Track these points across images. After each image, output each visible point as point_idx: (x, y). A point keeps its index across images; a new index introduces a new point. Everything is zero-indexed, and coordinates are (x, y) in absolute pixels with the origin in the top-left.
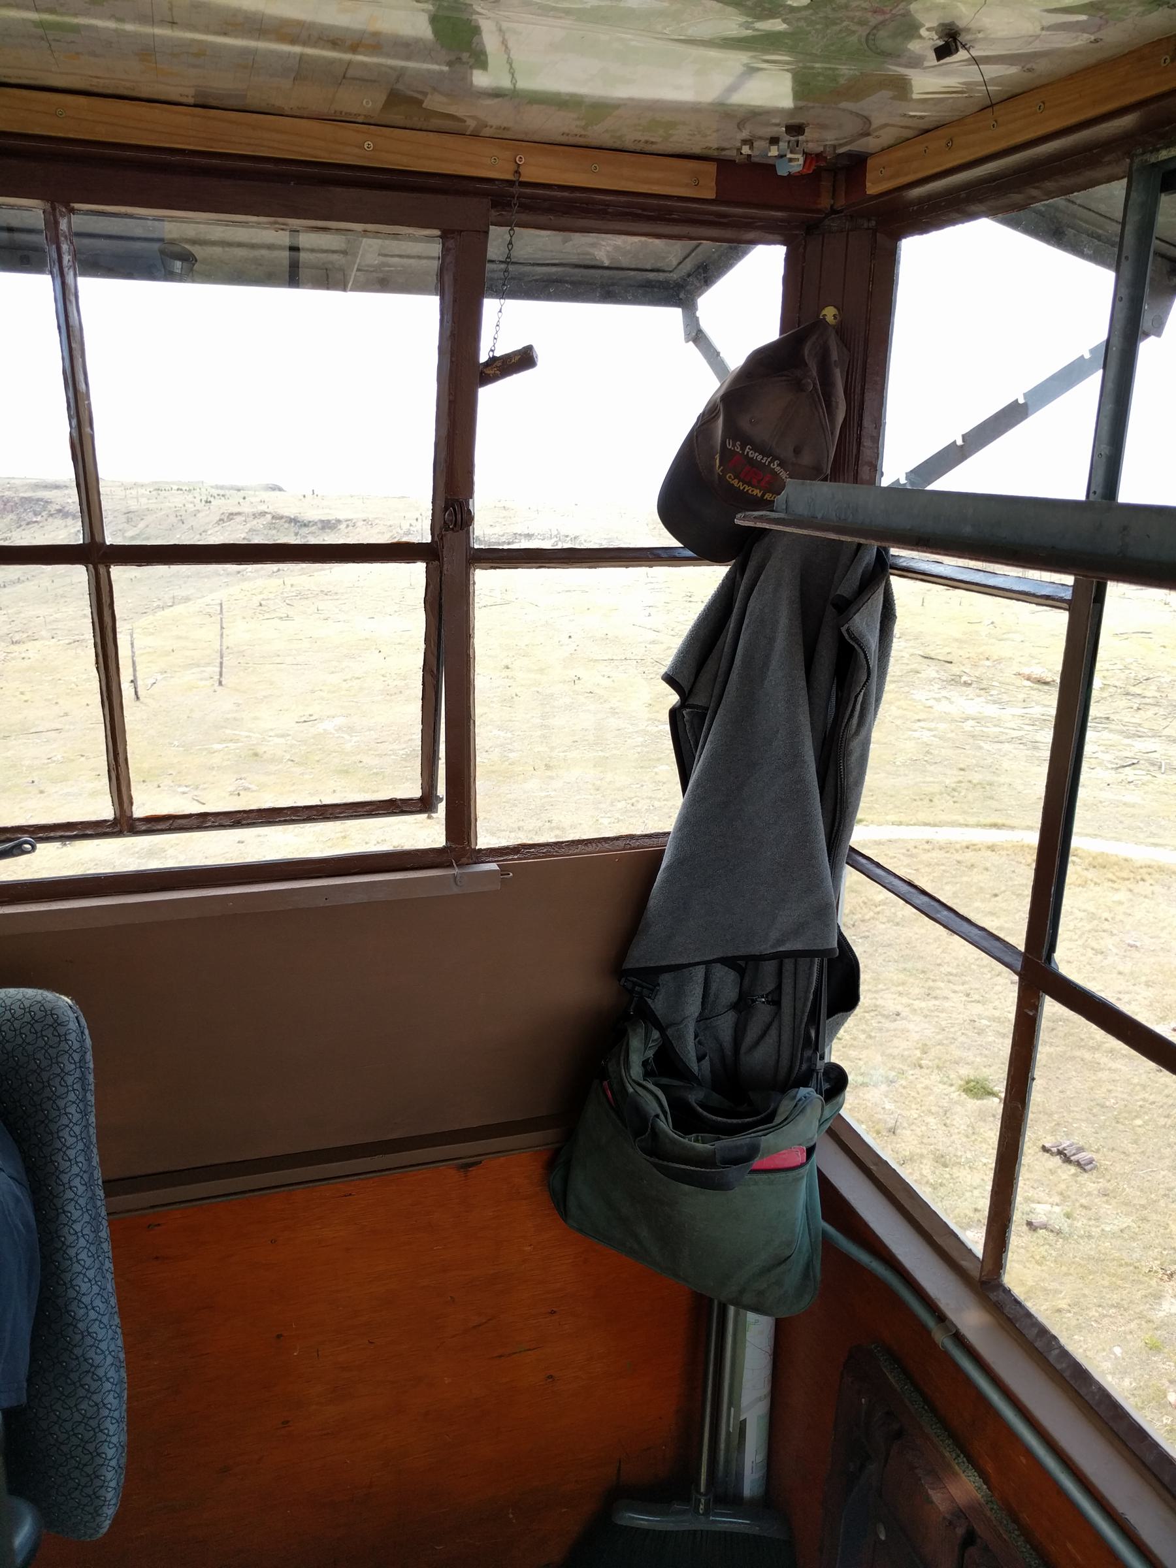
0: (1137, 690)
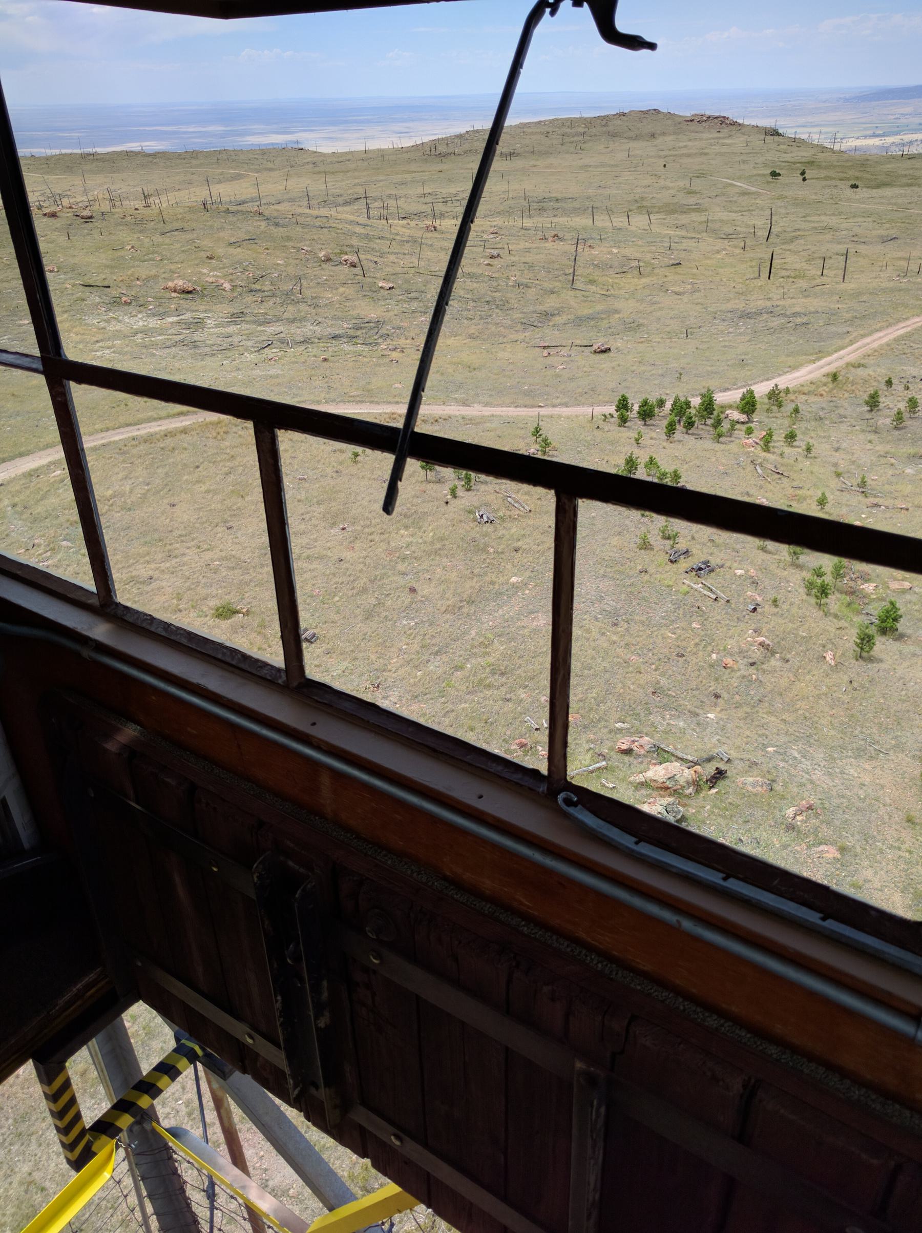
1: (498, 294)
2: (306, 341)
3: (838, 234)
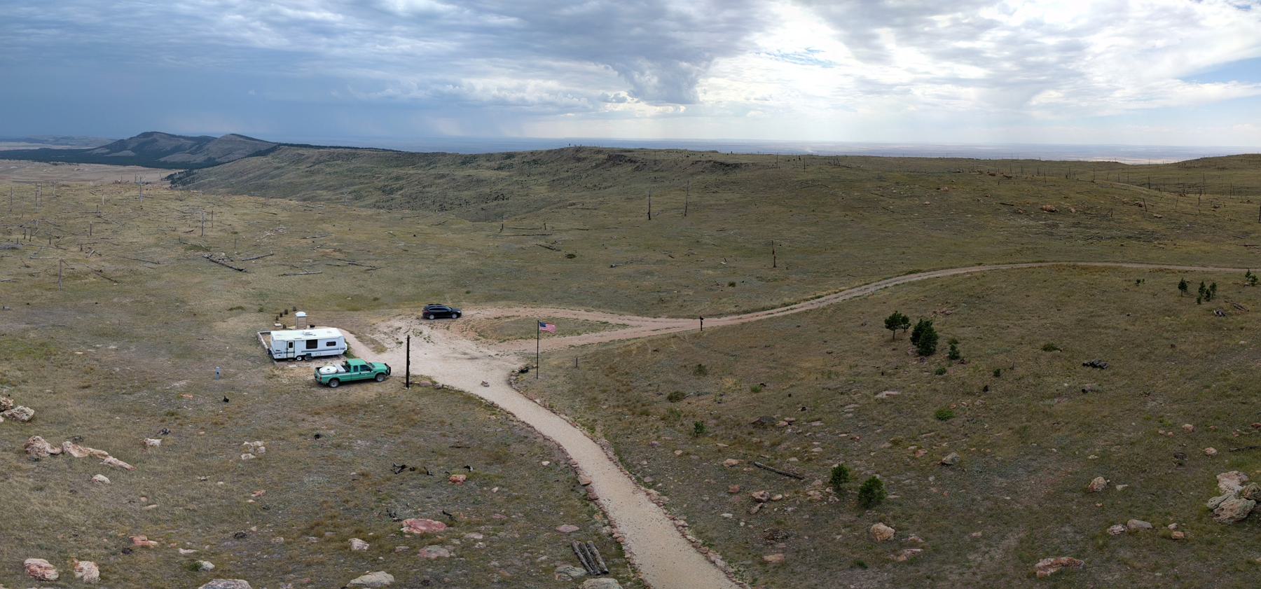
0: (1089, 212)
2: (1112, 238)
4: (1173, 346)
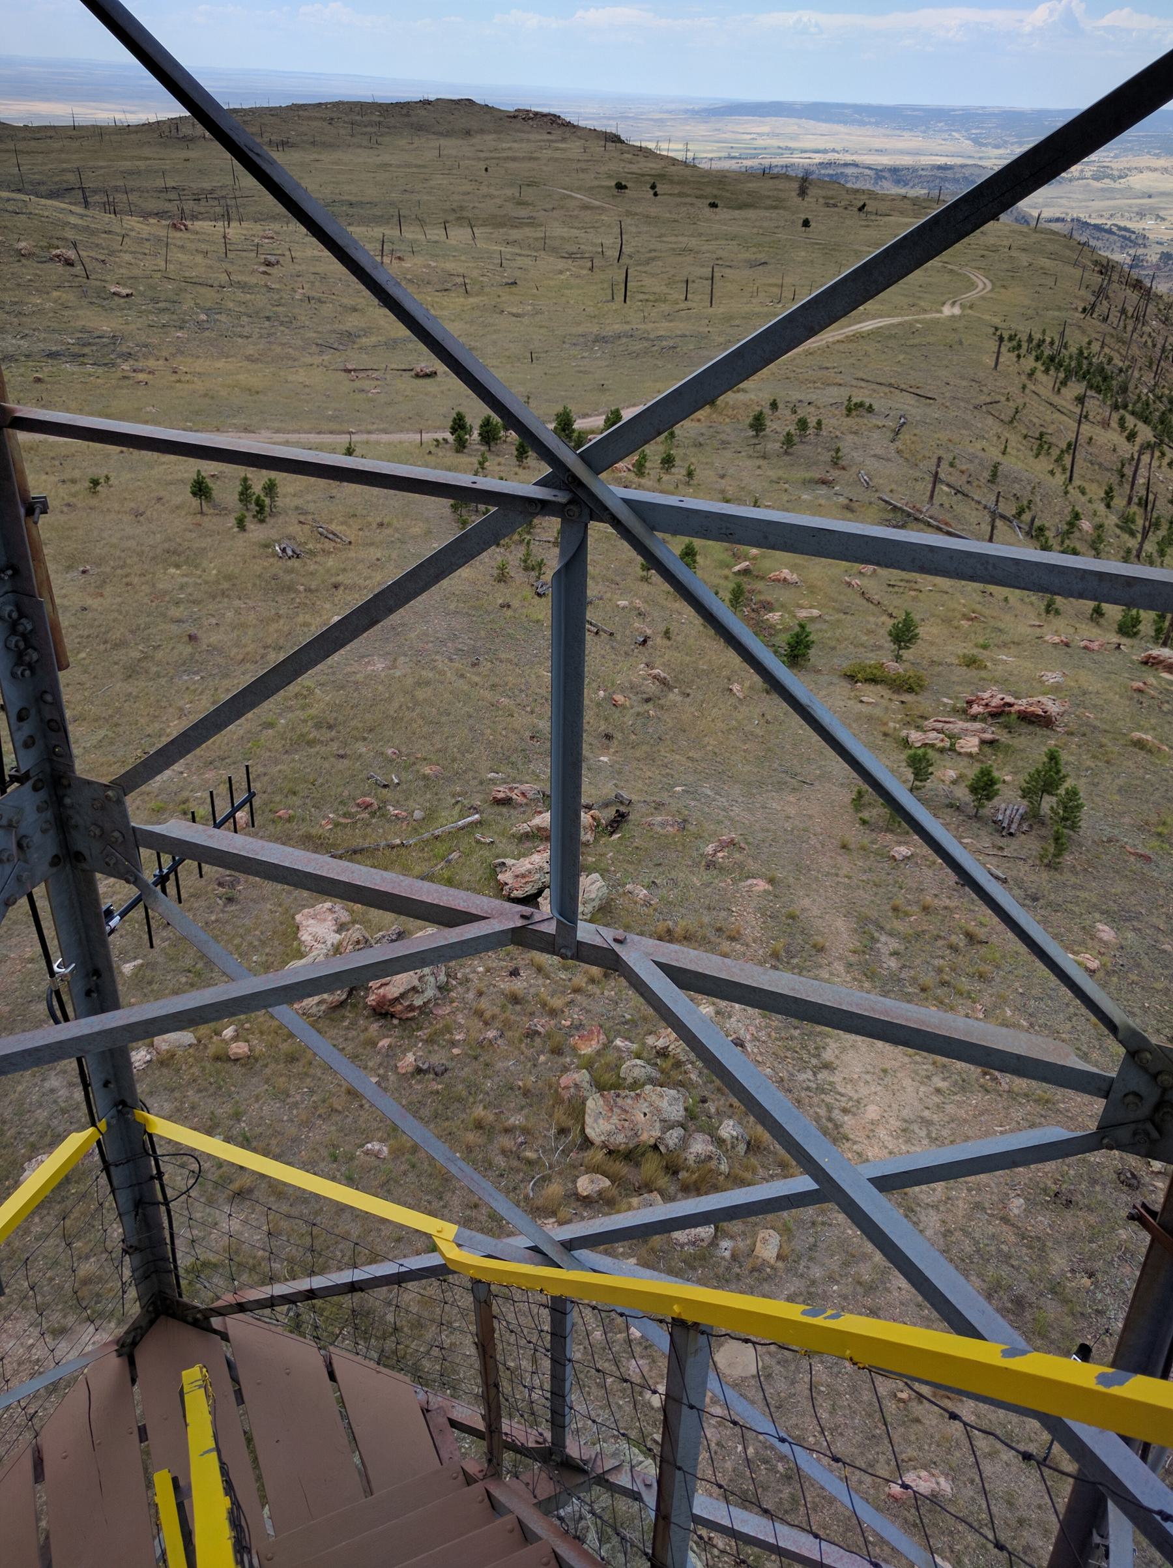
1: (280, 309)
3: (700, 256)
4: (192, 638)
